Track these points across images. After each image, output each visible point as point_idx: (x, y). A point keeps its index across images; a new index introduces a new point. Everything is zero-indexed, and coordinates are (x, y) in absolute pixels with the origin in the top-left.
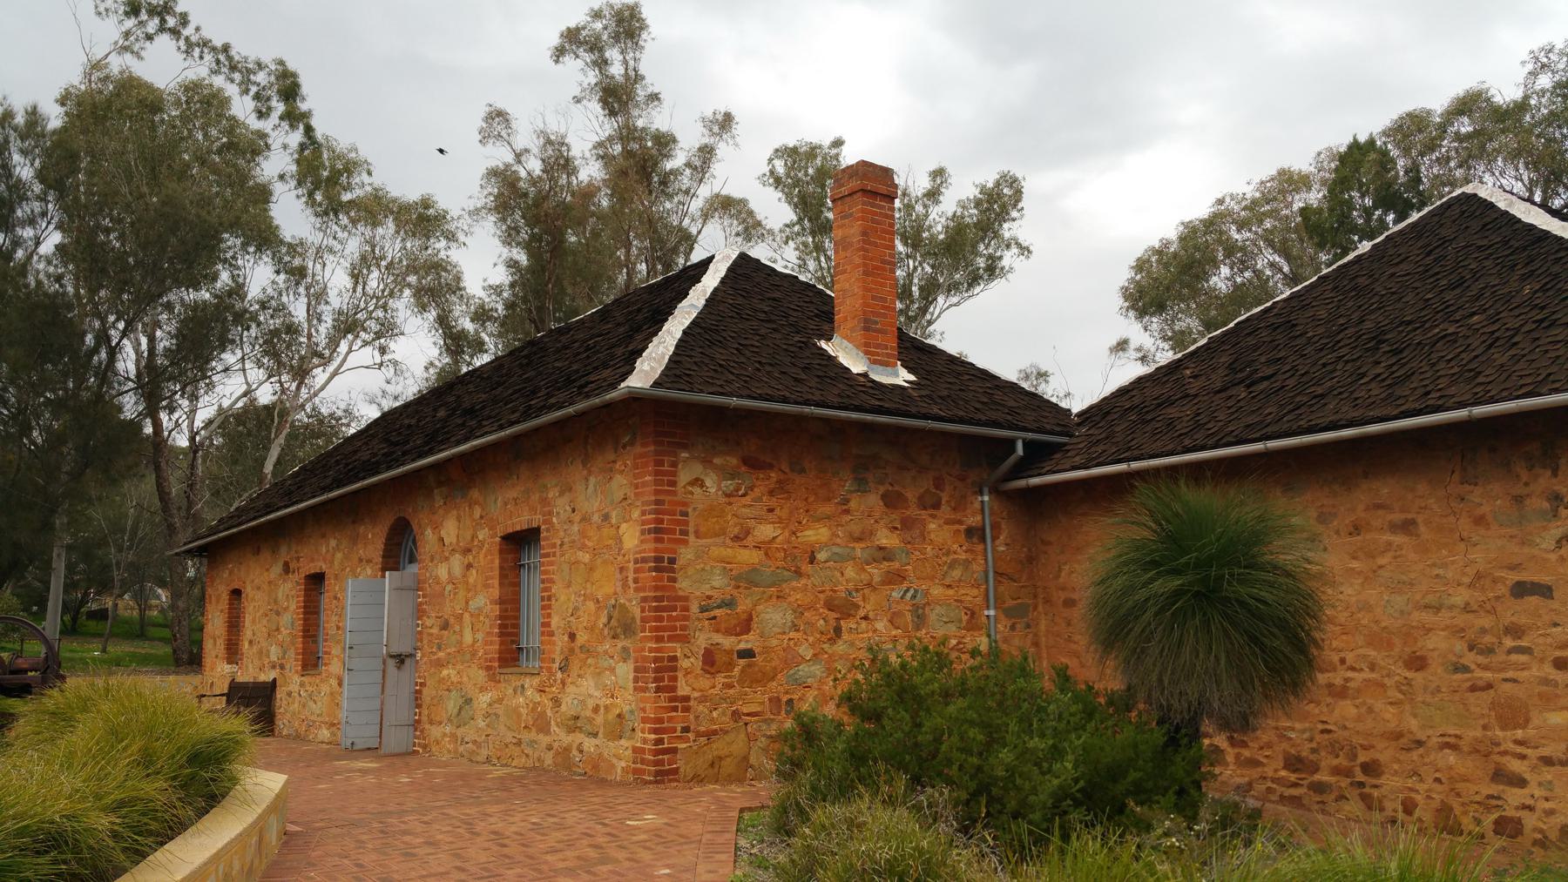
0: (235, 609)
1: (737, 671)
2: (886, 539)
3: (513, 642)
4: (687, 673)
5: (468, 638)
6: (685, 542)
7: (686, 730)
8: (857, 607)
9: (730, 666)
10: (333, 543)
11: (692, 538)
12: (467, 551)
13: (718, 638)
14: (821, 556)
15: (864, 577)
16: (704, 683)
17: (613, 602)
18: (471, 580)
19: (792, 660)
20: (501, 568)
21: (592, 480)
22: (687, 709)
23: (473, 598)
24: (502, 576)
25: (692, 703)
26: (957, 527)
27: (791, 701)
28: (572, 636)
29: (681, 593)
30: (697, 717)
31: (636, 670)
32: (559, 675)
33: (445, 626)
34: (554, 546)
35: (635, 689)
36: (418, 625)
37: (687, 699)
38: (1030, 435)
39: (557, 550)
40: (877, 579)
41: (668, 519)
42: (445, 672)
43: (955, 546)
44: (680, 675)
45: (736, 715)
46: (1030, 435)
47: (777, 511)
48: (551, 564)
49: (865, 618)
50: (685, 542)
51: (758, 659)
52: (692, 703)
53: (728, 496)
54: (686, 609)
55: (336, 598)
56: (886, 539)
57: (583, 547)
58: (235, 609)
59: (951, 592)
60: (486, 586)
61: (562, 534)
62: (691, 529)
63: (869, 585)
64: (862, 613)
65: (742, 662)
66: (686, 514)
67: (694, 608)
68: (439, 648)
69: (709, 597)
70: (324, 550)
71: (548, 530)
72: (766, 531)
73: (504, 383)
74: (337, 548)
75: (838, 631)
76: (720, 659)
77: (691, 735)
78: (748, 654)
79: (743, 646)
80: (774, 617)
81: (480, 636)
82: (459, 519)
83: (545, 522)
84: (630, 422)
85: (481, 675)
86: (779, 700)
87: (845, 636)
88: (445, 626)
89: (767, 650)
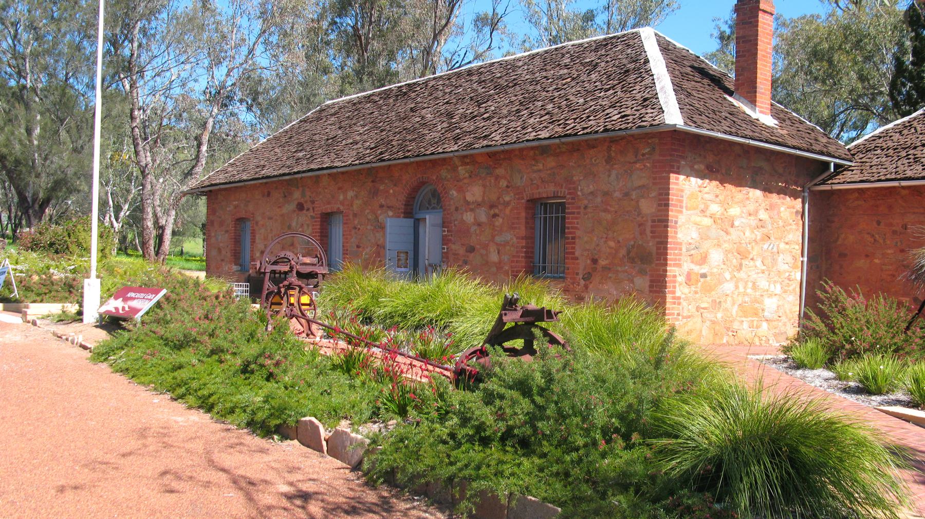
1: (700, 284)
2: (763, 215)
3: (531, 262)
4: (680, 284)
6: (681, 212)
7: (678, 314)
8: (750, 253)
9: (697, 281)
11: (684, 210)
12: (492, 206)
13: (693, 266)
14: (736, 223)
15: (753, 236)
16: (686, 290)
17: (632, 243)
19: (720, 281)
20: (526, 218)
21: (614, 173)
22: (679, 304)
24: (527, 223)
25: (682, 301)
26: (792, 210)
27: (720, 302)
28: (595, 261)
29: (679, 240)
30: (683, 308)
31: (651, 281)
35: (650, 291)
36: (444, 249)
37: (679, 298)
38: (837, 161)
39: (582, 210)
40: (759, 237)
43: (791, 221)
44: (677, 285)
45: (698, 308)
46: (837, 161)
47: (720, 197)
49: (752, 259)
50: (681, 212)
51: (709, 278)
52: (682, 301)
53: (700, 187)
54: (681, 249)
56: (763, 215)
57: (606, 211)
59: (787, 247)
62: (684, 205)
63: (755, 241)
64: (751, 256)
65: (702, 280)
66: (682, 197)
67: (684, 250)
69: (690, 244)
72: (715, 208)
75: (741, 265)
76: (693, 277)
77: (680, 317)
78: (704, 276)
79: (703, 271)
80: (716, 257)
84: (650, 141)
86: (716, 301)
87: (744, 269)
89: (712, 274)
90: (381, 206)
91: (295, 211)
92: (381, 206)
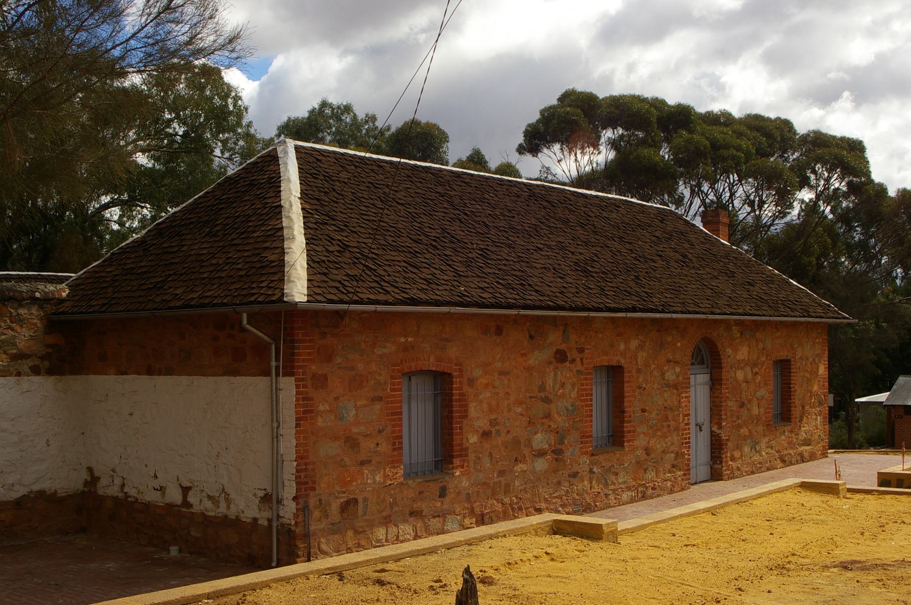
0: (717, 397)
5: (755, 411)
10: (634, 343)
12: (755, 365)
18: (757, 381)
23: (758, 391)
32: (798, 424)
33: (742, 405)
34: (796, 369)
38: (256, 308)
41: (302, 333)
42: (742, 431)
46: (256, 308)
48: (796, 376)
55: (640, 388)
58: (717, 397)
60: (766, 384)
61: (799, 364)
68: (738, 418)
70: (622, 347)
71: (795, 361)
73: (332, 188)
74: (641, 347)
81: (762, 410)
82: (749, 346)
83: (793, 357)
85: (760, 428)
88: (742, 405)
90: (669, 361)
91: (550, 363)
92: (669, 361)
